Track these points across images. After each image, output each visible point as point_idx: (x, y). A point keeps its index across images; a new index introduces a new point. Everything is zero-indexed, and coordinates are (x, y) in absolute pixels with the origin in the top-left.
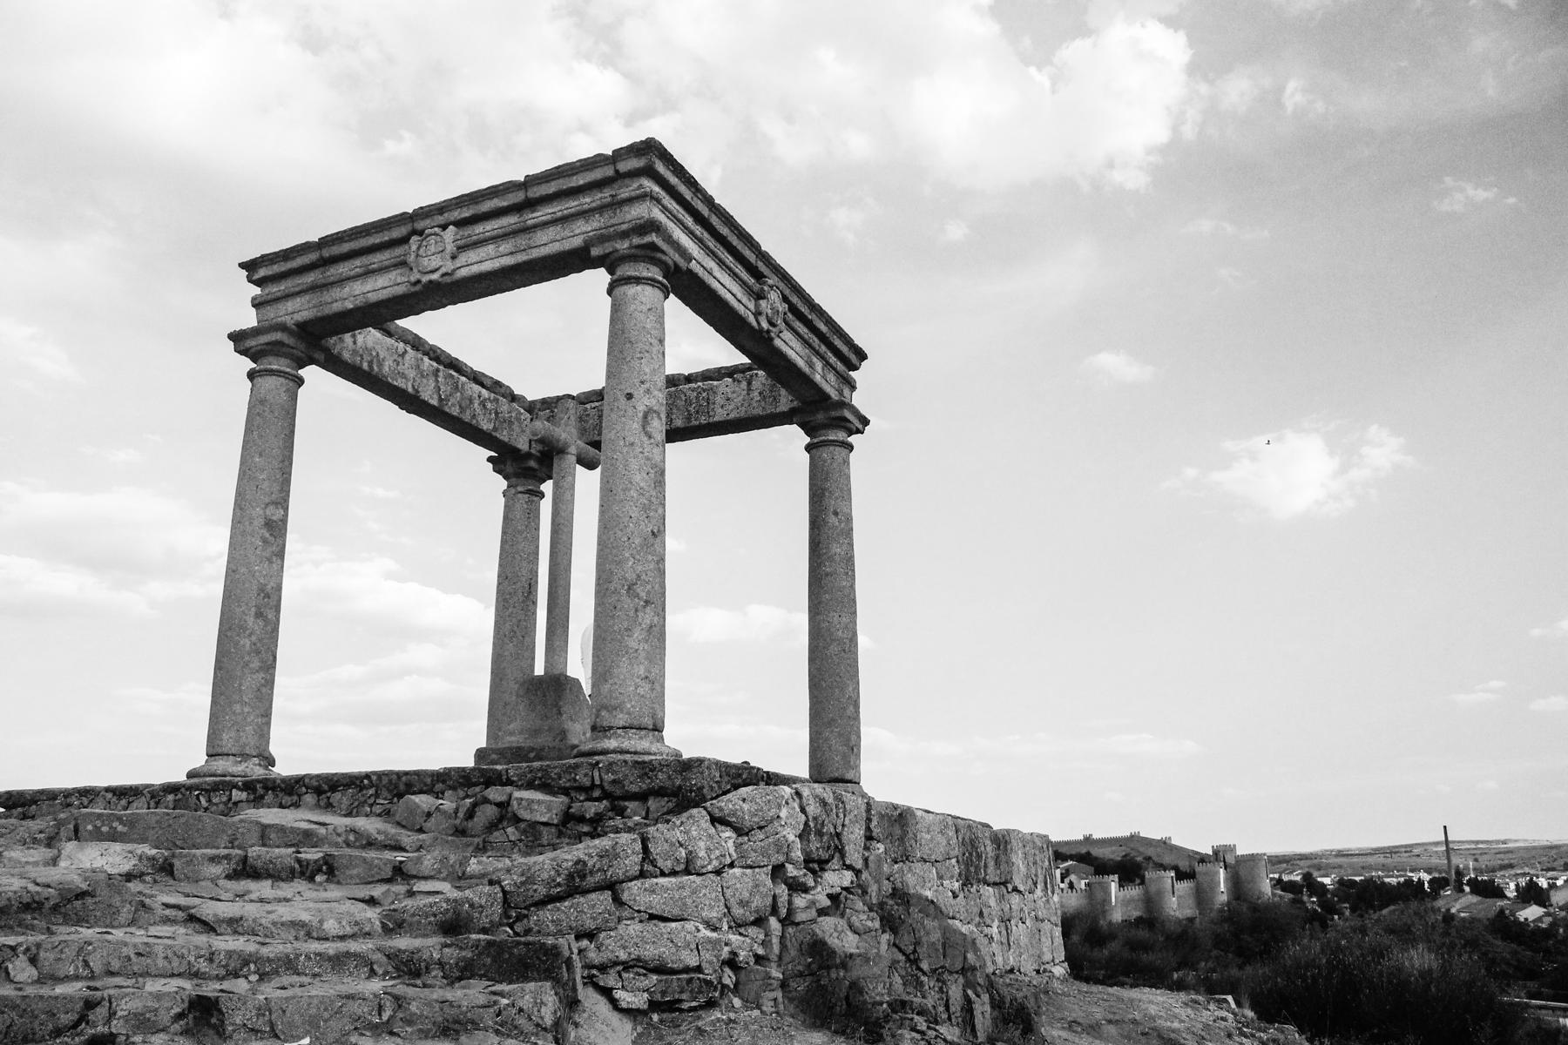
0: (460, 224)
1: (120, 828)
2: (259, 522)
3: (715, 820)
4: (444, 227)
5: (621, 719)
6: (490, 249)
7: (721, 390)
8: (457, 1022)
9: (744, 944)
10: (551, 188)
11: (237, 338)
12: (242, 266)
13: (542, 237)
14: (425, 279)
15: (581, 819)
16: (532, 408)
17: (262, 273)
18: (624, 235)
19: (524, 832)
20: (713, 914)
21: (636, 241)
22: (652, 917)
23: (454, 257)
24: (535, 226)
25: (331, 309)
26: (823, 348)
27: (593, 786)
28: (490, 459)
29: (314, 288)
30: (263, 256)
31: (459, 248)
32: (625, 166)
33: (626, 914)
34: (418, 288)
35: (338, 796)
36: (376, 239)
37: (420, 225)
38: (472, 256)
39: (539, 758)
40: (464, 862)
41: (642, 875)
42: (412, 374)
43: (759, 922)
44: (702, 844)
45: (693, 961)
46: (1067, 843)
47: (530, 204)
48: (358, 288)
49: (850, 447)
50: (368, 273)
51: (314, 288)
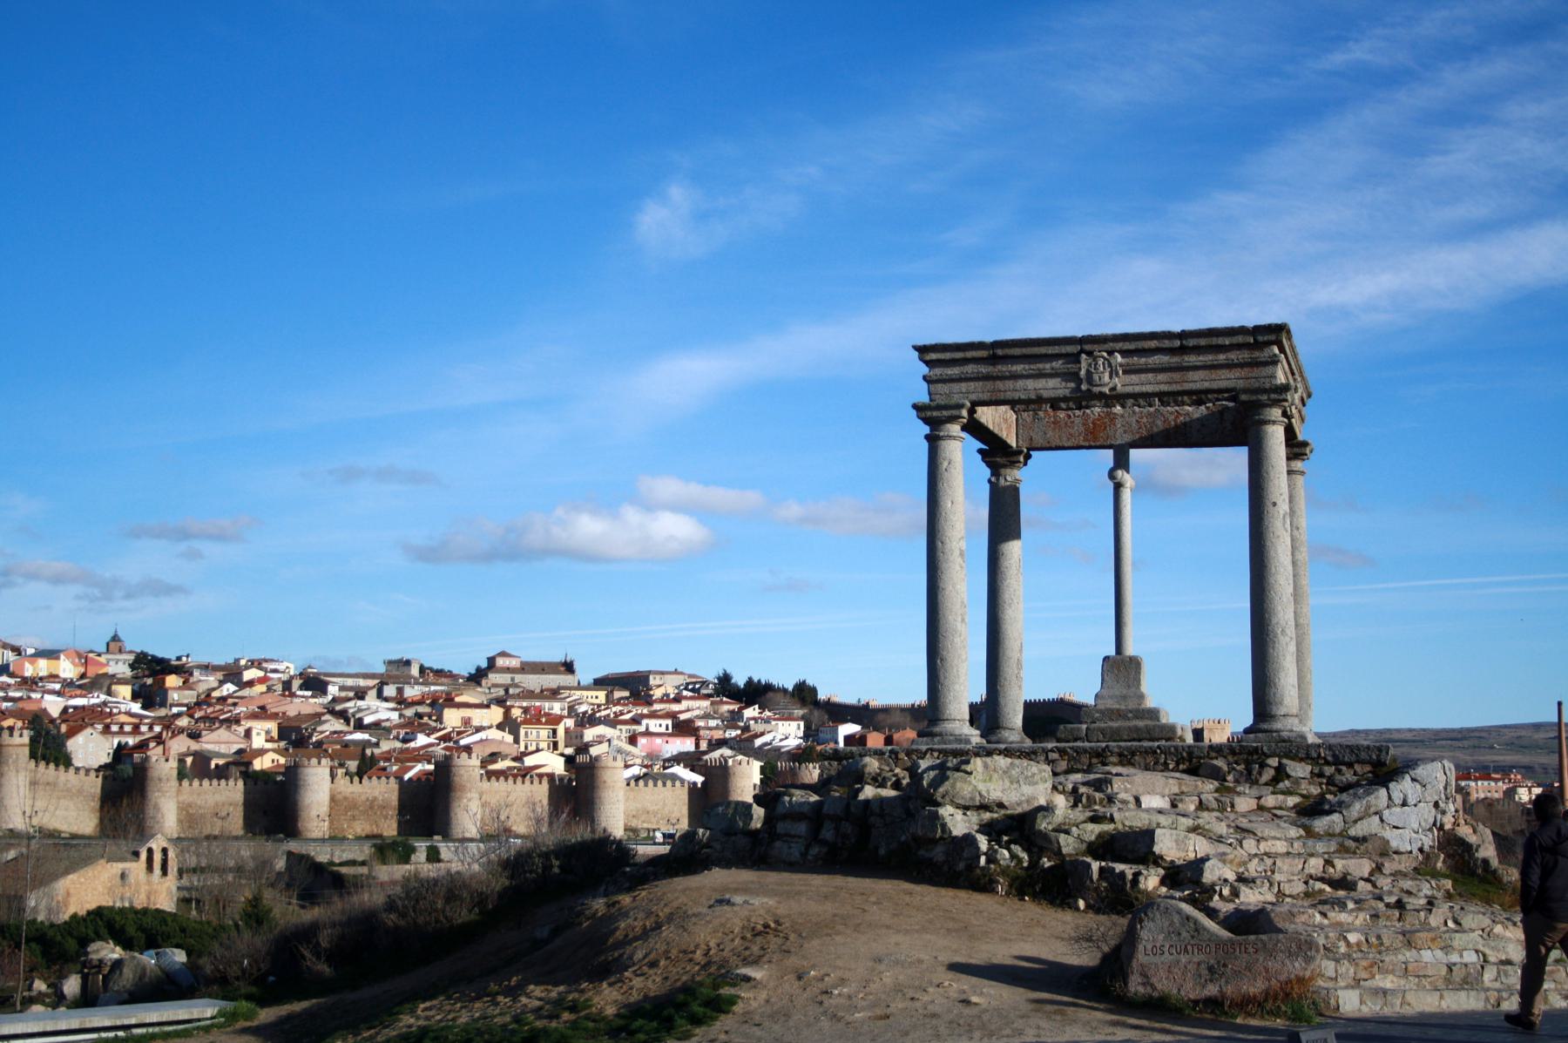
2: (957, 553)
3: (1413, 780)
11: (918, 408)
13: (1192, 375)
17: (933, 356)
20: (1416, 826)
26: (1222, 357)
37: (1087, 347)
38: (1134, 378)
39: (1137, 717)
46: (1335, 735)
47: (1183, 350)
48: (1031, 384)
50: (1041, 375)
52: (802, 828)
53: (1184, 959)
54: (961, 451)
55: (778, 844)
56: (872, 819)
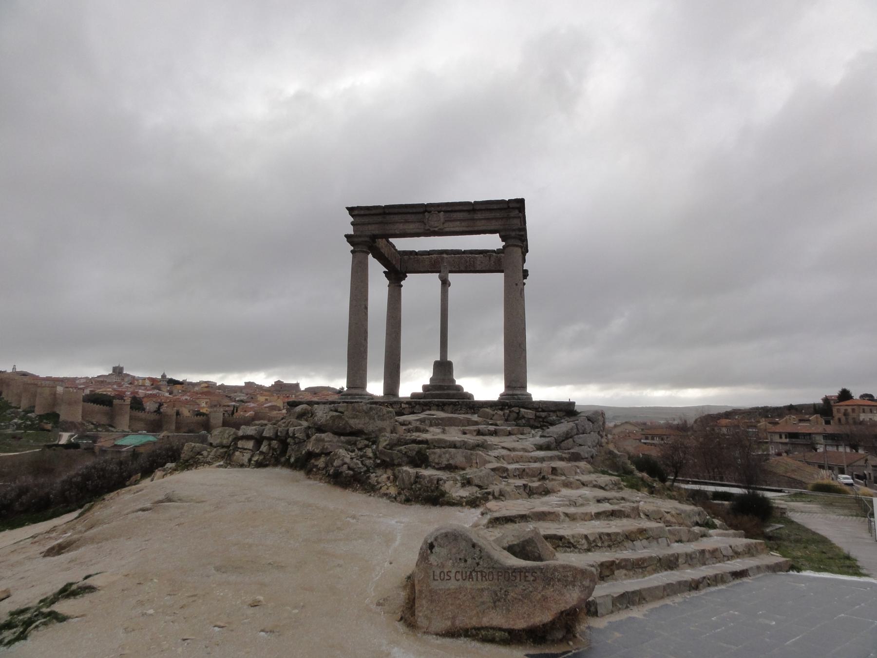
0: (445, 212)
4: (439, 212)
6: (458, 223)
8: (624, 472)
9: (594, 451)
10: (483, 207)
11: (347, 236)
14: (432, 229)
15: (540, 417)
17: (356, 212)
18: (514, 230)
21: (518, 233)
28: (385, 272)
29: (381, 223)
37: (428, 209)
38: (451, 224)
49: (524, 284)
50: (407, 222)
51: (381, 223)
52: (250, 444)
53: (468, 584)
54: (376, 270)
55: (237, 453)
56: (289, 440)
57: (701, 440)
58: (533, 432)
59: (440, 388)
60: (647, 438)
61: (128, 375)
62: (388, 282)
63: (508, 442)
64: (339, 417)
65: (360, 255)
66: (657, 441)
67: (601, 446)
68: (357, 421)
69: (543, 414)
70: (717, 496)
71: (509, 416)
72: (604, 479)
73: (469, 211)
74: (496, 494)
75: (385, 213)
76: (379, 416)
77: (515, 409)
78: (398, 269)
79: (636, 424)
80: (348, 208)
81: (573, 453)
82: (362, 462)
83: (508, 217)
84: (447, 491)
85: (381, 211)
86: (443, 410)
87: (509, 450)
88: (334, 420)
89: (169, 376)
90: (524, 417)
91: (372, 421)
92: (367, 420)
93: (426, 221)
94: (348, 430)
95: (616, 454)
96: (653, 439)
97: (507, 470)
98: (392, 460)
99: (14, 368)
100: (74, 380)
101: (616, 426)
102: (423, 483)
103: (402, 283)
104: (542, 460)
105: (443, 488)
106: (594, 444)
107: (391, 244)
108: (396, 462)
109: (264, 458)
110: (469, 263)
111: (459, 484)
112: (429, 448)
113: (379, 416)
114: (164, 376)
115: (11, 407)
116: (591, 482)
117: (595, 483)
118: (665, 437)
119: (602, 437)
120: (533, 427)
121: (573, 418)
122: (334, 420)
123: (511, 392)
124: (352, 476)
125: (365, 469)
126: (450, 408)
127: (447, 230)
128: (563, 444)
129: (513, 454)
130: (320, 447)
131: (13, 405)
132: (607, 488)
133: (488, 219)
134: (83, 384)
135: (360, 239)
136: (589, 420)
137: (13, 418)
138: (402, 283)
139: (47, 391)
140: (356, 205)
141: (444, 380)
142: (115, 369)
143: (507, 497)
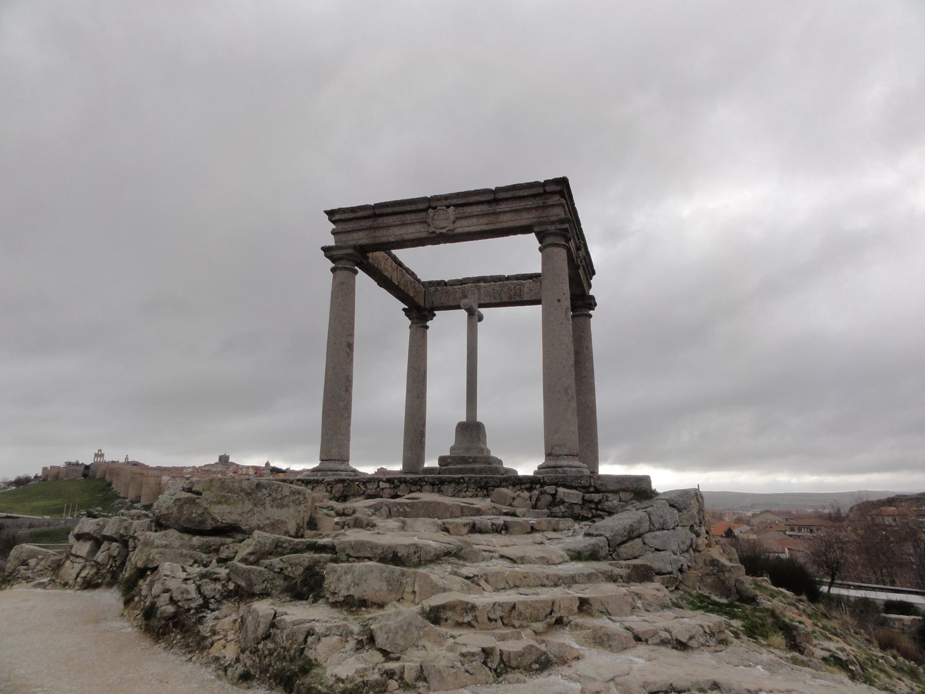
0: (456, 206)
1: (408, 509)
4: (448, 207)
5: (566, 451)
6: (474, 220)
7: (527, 285)
8: (735, 601)
9: (684, 560)
10: (509, 195)
11: (326, 250)
12: (326, 212)
14: (438, 231)
15: (591, 502)
16: (424, 284)
17: (337, 217)
18: (553, 223)
19: (567, 508)
21: (559, 226)
22: (657, 550)
23: (454, 222)
24: (500, 213)
25: (366, 240)
27: (590, 486)
28: (404, 310)
29: (370, 228)
30: (339, 209)
31: (457, 218)
32: (549, 189)
33: (648, 548)
34: (434, 235)
35: (446, 487)
36: (409, 208)
37: (433, 204)
38: (464, 222)
40: (558, 524)
41: (650, 531)
42: (390, 269)
43: (687, 551)
44: (669, 516)
45: (670, 569)
47: (496, 201)
49: (590, 316)
50: (404, 224)
51: (370, 228)
57: (861, 532)
58: (577, 526)
59: (464, 460)
60: (792, 530)
61: (234, 464)
62: (408, 322)
63: (518, 544)
64: (192, 502)
65: (343, 274)
66: (805, 533)
67: (696, 550)
68: (225, 508)
69: (596, 497)
70: (891, 606)
71: (538, 499)
72: (692, 622)
73: (488, 202)
74: (409, 676)
75: (375, 216)
76: (274, 500)
77: (550, 489)
78: (421, 303)
79: (779, 514)
80: (327, 212)
81: (635, 567)
82: (199, 588)
83: (547, 210)
84: (321, 659)
85: (370, 212)
86: (440, 491)
87: (513, 561)
88: (181, 507)
89: (272, 465)
90: (562, 502)
91: (260, 509)
92: (249, 506)
93: (429, 221)
94: (210, 524)
95: (723, 566)
96: (800, 530)
97: (473, 608)
98: (251, 584)
99: (127, 458)
100: (182, 469)
101: (754, 516)
102: (278, 640)
103: (429, 323)
104: (571, 580)
105: (310, 654)
106: (684, 547)
107: (395, 259)
108: (258, 589)
109: (96, 573)
110: (510, 291)
111: (352, 644)
112: (335, 561)
113: (274, 500)
114: (267, 464)
115: (119, 497)
116: (655, 633)
117: (665, 635)
118: (814, 529)
119: (698, 535)
120: (578, 518)
121: (645, 503)
122: (181, 507)
123: (552, 463)
124: (175, 615)
125: (201, 601)
126: (450, 489)
127: (459, 230)
128: (622, 549)
129: (521, 568)
130: (144, 558)
131: (121, 495)
132: (693, 643)
133: (516, 211)
134: (190, 473)
135: (342, 252)
136: (672, 506)
137: (120, 508)
138: (429, 323)
139: (152, 481)
140: (336, 207)
141: (469, 449)
142: (221, 458)
143: (434, 683)
